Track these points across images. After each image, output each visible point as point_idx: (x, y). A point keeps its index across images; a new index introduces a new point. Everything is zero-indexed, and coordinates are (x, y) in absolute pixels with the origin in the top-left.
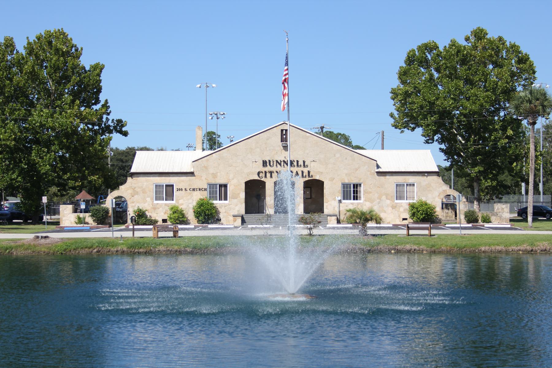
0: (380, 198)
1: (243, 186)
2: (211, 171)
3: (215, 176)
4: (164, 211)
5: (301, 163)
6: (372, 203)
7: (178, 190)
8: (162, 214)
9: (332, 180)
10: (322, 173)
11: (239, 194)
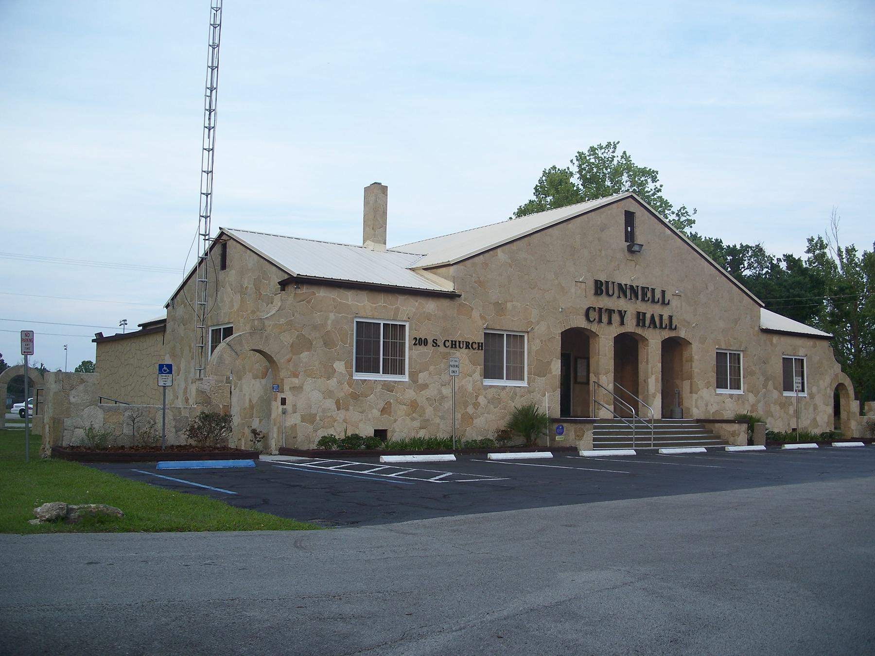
0: (765, 386)
1: (557, 346)
3: (500, 308)
4: (381, 405)
5: (658, 295)
7: (420, 342)
8: (376, 412)
9: (703, 340)
11: (549, 363)
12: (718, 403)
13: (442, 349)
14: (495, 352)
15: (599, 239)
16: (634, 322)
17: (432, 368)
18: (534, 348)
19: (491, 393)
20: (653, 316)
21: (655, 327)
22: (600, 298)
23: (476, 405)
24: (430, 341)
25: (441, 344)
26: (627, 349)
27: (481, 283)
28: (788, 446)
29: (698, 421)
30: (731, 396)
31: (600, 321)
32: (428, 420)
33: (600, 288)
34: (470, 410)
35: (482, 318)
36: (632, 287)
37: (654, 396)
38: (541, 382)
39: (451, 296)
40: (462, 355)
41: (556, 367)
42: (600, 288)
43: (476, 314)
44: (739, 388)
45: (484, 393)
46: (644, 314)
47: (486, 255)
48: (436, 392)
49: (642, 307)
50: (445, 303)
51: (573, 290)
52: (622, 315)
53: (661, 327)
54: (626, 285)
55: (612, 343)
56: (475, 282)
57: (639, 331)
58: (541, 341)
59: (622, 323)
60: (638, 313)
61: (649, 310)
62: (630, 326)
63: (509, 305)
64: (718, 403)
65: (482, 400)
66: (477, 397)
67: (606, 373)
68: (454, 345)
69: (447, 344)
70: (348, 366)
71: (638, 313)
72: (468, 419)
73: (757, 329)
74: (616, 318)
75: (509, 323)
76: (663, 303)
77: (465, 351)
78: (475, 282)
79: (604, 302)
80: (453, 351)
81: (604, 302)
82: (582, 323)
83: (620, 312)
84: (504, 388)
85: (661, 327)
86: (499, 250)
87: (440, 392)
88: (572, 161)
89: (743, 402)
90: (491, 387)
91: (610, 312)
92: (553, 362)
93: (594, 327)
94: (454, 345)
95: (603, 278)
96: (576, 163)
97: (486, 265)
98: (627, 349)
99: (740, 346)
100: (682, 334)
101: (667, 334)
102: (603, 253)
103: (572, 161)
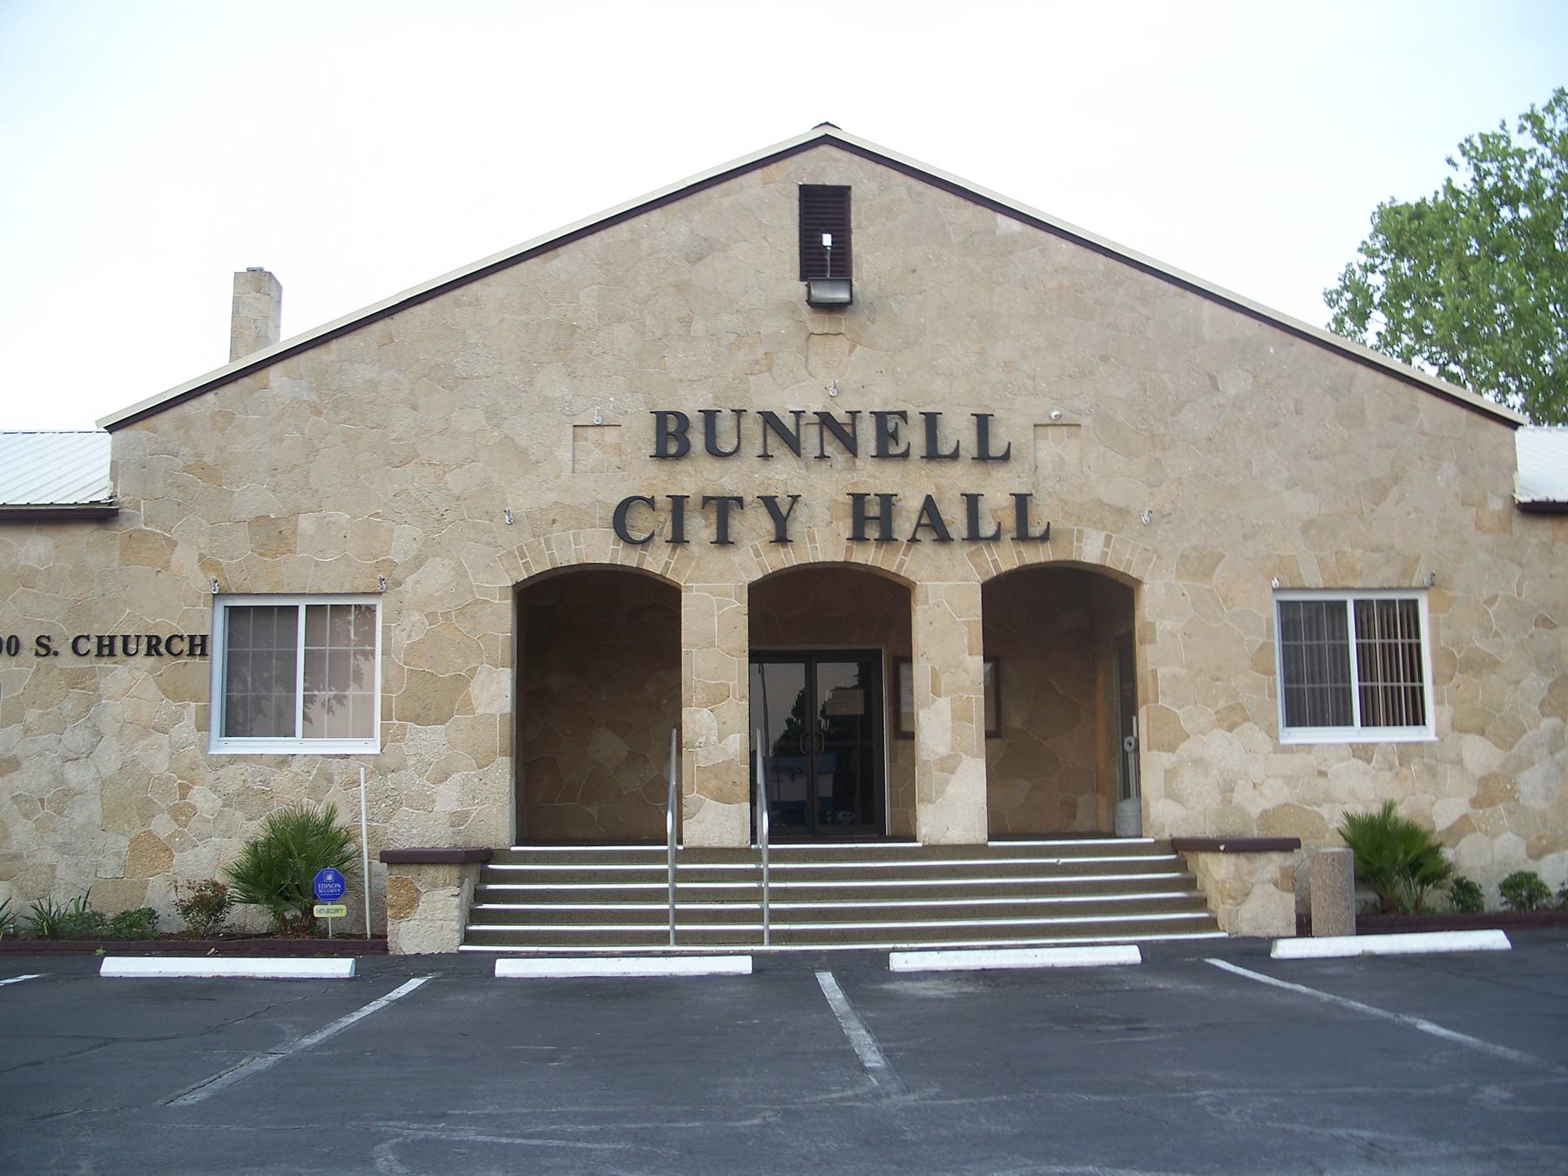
2: (253, 498)
3: (273, 534)
6: (1505, 743)
9: (1201, 564)
10: (1123, 512)
12: (1289, 779)
13: (67, 661)
14: (264, 655)
15: (681, 288)
16: (845, 528)
17: (31, 715)
18: (401, 639)
19: (232, 779)
20: (929, 505)
21: (944, 538)
22: (683, 466)
23: (183, 813)
24: (28, 642)
25: (65, 649)
26: (831, 630)
27: (205, 471)
28: (113, 966)
29: (1176, 845)
30: (1362, 752)
31: (678, 539)
32: (16, 857)
33: (671, 438)
34: (162, 826)
35: (206, 563)
36: (825, 420)
37: (948, 765)
38: (428, 740)
39: (99, 515)
40: (131, 679)
41: (495, 691)
42: (671, 438)
43: (185, 559)
44: (1418, 719)
45: (211, 777)
46: (887, 501)
47: (230, 390)
48: (45, 779)
49: (874, 478)
50: (82, 537)
51: (565, 455)
52: (780, 514)
53: (973, 536)
54: (798, 414)
55: (738, 607)
56: (187, 469)
57: (868, 556)
58: (431, 616)
59: (782, 539)
60: (859, 500)
61: (911, 485)
62: (823, 541)
63: (306, 523)
64: (1289, 779)
65: (202, 798)
66: (184, 790)
67: (716, 699)
68: (106, 647)
69: (84, 646)
70: (203, 725)
71: (859, 500)
72: (151, 850)
73: (1497, 505)
74: (753, 526)
75: (307, 572)
76: (983, 456)
77: (143, 663)
78: (187, 469)
79: (698, 477)
80: (105, 663)
81: (698, 477)
82: (602, 549)
83: (769, 502)
84: (284, 761)
85: (973, 536)
86: (274, 372)
87: (58, 778)
88: (1449, 161)
89: (1432, 772)
90: (235, 759)
91: (723, 507)
92: (479, 678)
93: (656, 561)
94: (106, 647)
95: (691, 404)
96: (1462, 161)
97: (225, 418)
98: (831, 630)
99: (1407, 572)
100: (1091, 551)
101: (1007, 558)
102: (698, 326)
103: (1449, 161)
